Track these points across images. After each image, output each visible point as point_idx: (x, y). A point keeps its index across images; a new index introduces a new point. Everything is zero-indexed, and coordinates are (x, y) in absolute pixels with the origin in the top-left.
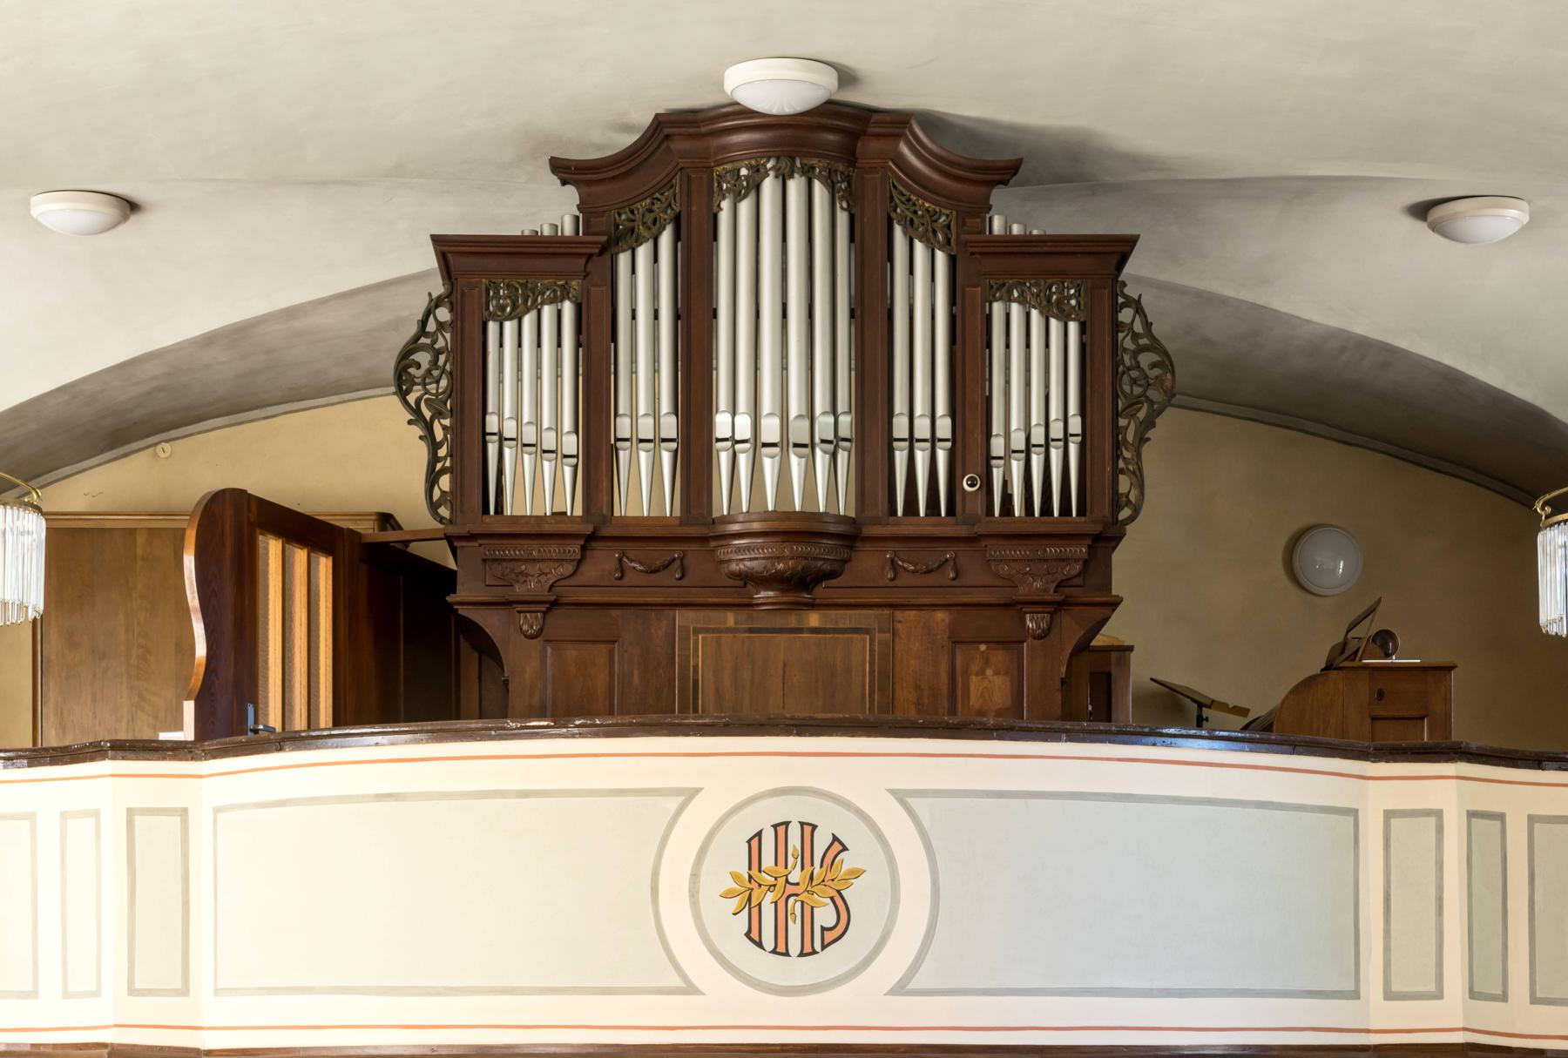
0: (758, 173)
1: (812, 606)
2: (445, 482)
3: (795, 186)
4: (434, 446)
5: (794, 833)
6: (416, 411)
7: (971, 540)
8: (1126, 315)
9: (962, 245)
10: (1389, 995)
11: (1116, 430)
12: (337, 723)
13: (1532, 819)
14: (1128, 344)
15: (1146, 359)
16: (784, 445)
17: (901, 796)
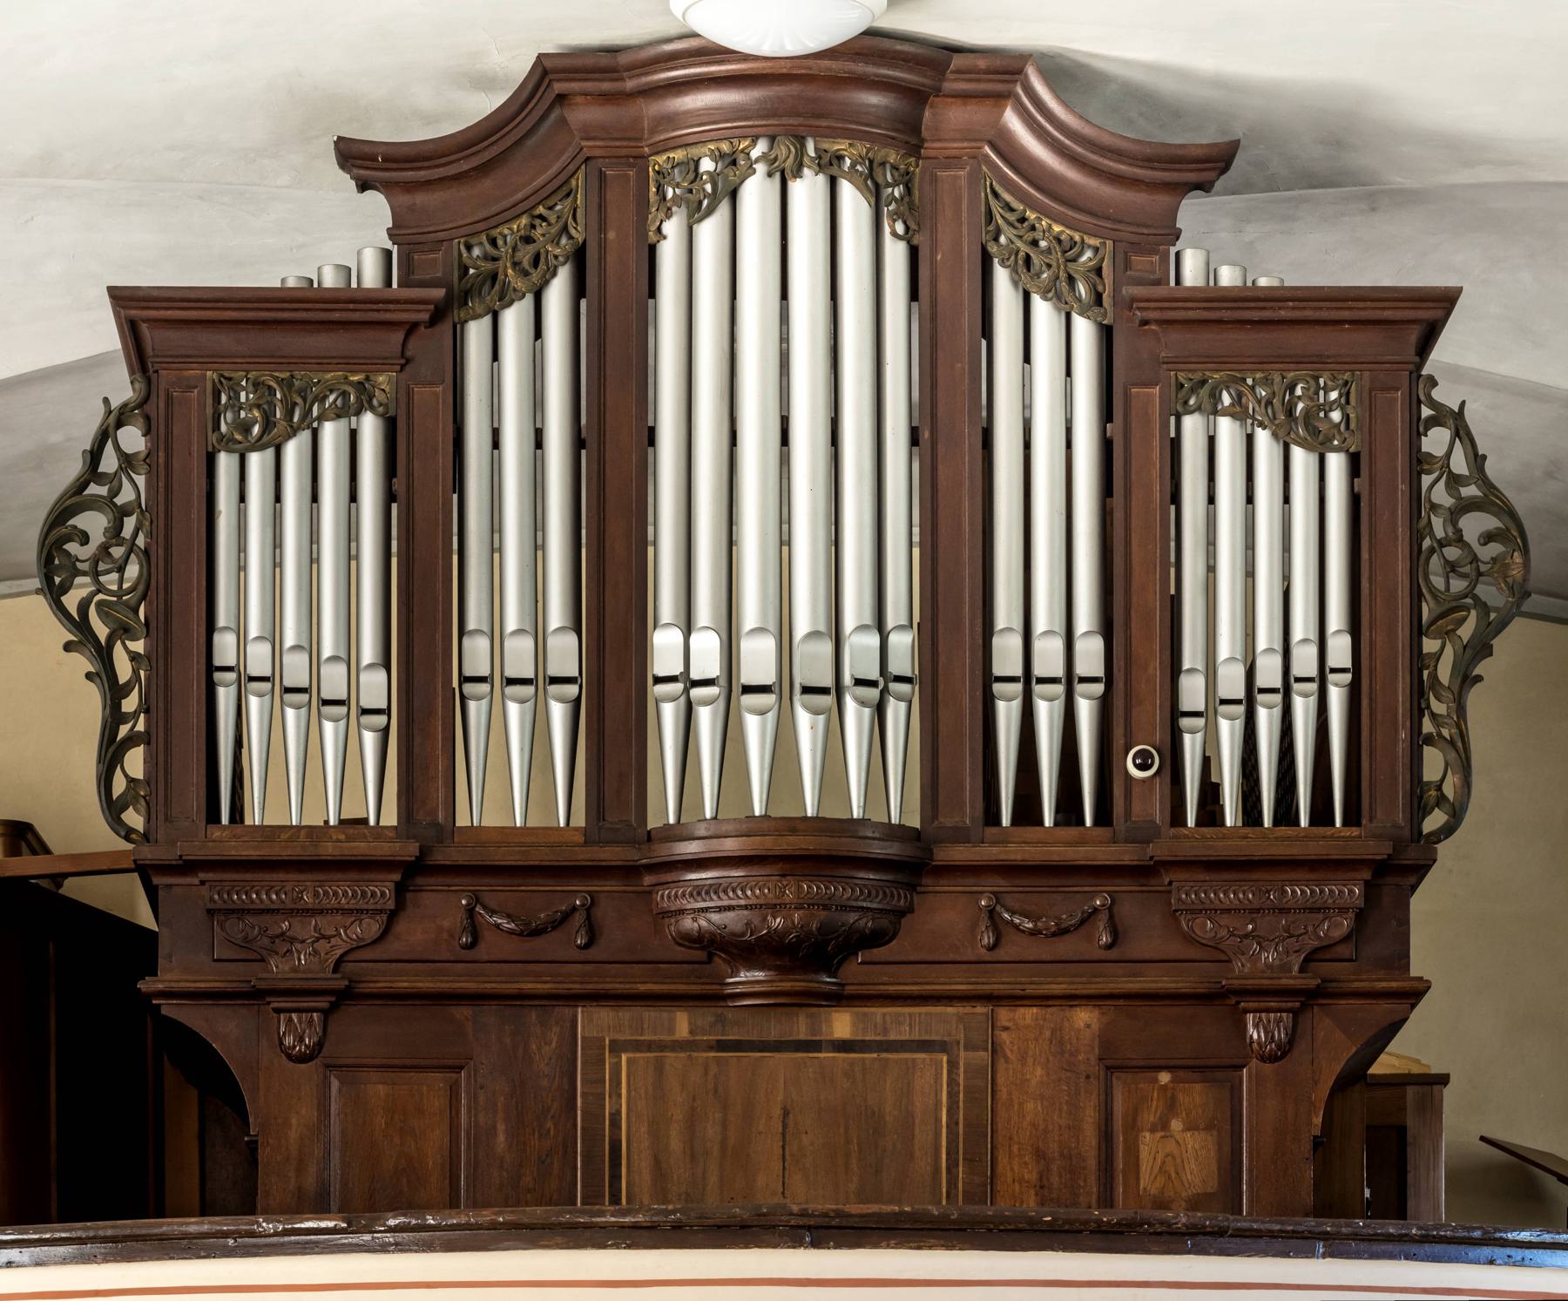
1: (839, 999)
2: (135, 762)
4: (114, 692)
6: (80, 625)
7: (1144, 872)
8: (1436, 441)
11: (1419, 661)
15: (1474, 525)
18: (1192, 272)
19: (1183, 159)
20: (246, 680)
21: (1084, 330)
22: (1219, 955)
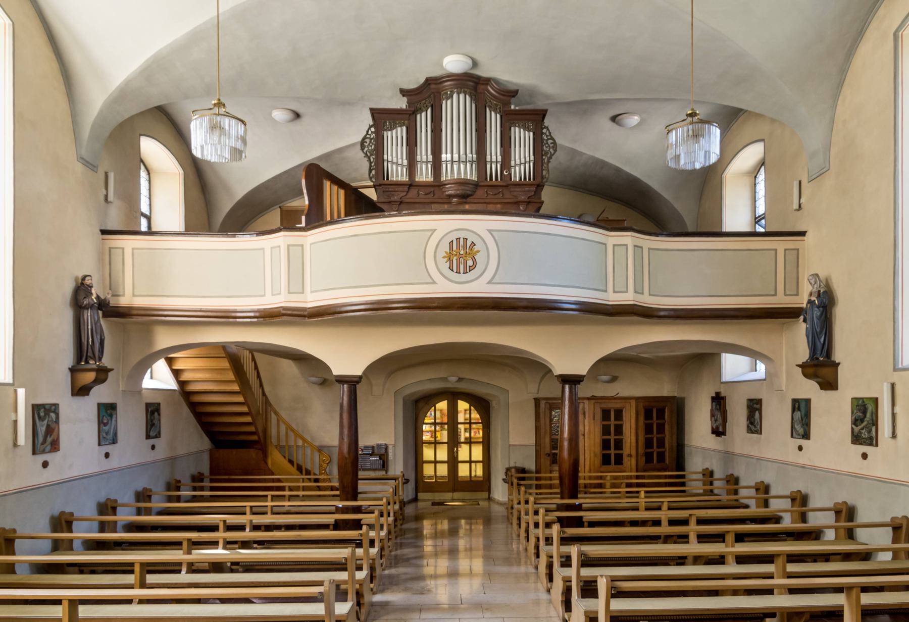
0: (452, 92)
1: (466, 203)
2: (373, 172)
3: (462, 96)
4: (371, 163)
5: (462, 240)
6: (366, 154)
7: (507, 186)
8: (544, 131)
9: (504, 112)
10: (614, 292)
11: (543, 160)
12: (346, 216)
13: (649, 249)
15: (550, 141)
18: (513, 107)
19: (511, 93)
20: (393, 163)
21: (498, 116)
22: (516, 197)
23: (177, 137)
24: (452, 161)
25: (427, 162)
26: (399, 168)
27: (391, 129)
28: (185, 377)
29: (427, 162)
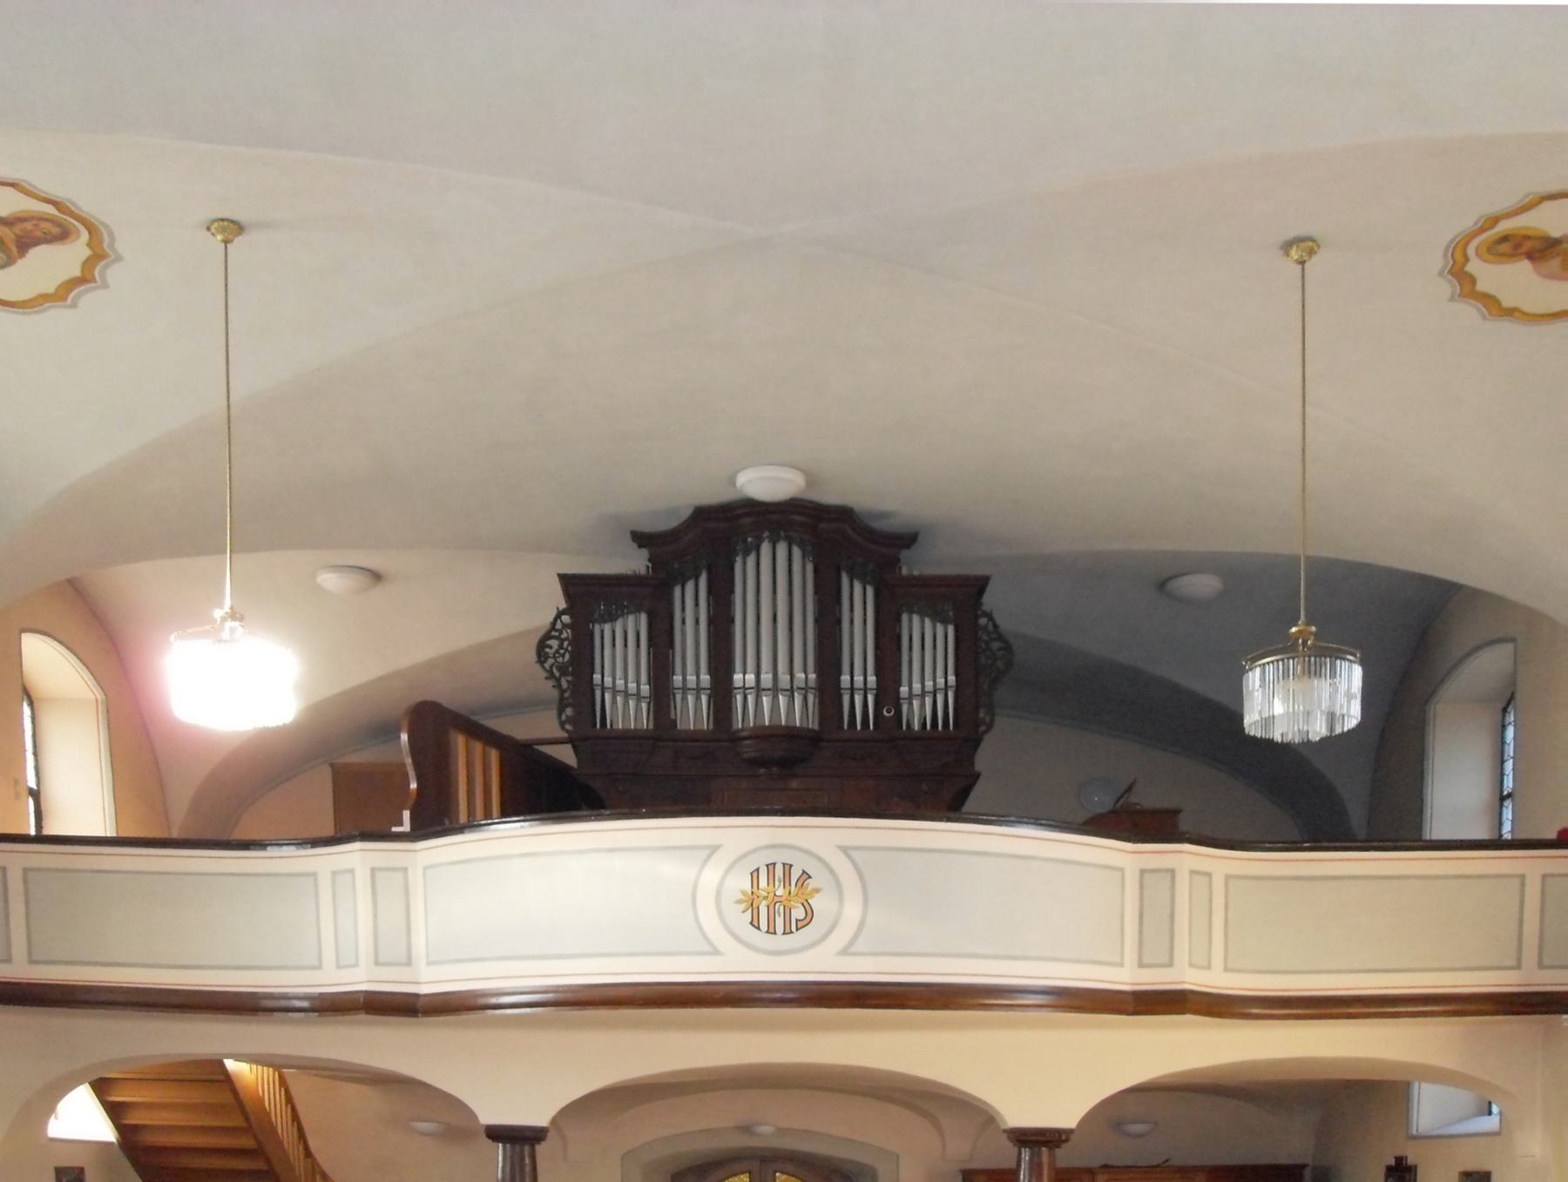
1: (795, 776)
4: (563, 692)
8: (983, 621)
14: (985, 637)
16: (775, 690)
17: (845, 850)
21: (870, 591)
23: (109, 644)
24: (758, 689)
25: (698, 690)
26: (632, 703)
27: (612, 619)
28: (132, 1119)
29: (698, 690)
